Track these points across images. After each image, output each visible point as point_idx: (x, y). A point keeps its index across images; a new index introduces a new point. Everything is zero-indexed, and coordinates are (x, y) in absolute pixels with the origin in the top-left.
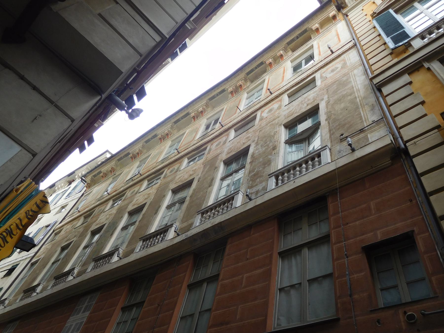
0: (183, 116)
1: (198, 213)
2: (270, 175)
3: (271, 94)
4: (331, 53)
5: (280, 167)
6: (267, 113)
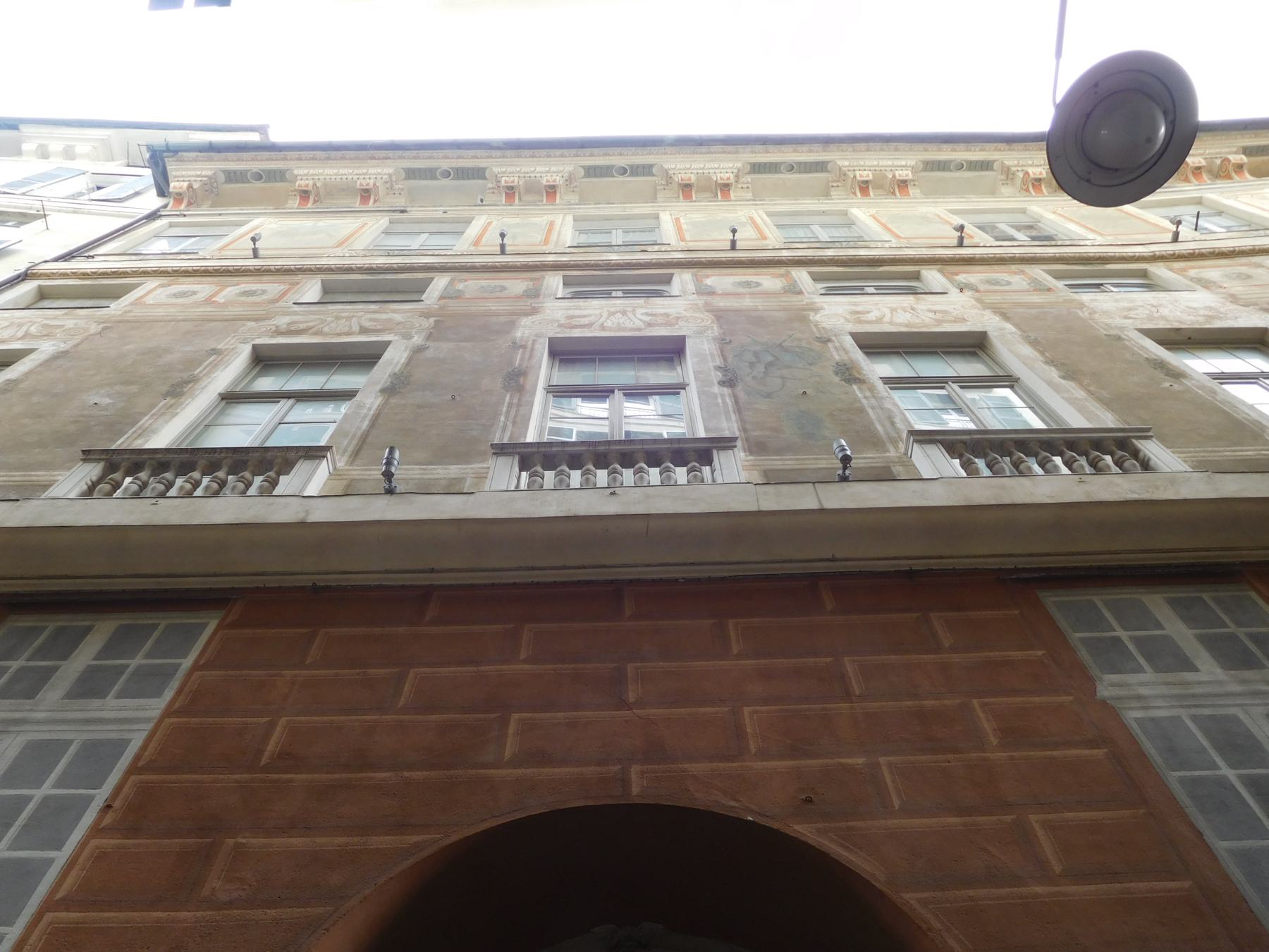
0: (799, 164)
1: (501, 450)
2: (501, 450)
3: (961, 245)
5: (531, 437)
6: (168, 296)
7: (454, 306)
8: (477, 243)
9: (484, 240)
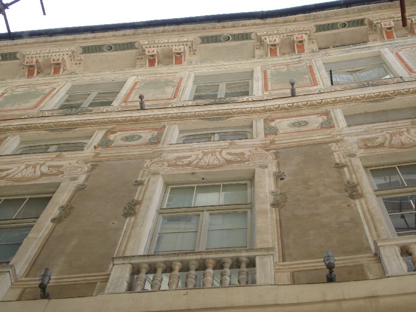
3: (293, 95)
4: (139, 108)
7: (104, 153)
8: (125, 101)
9: (130, 100)
